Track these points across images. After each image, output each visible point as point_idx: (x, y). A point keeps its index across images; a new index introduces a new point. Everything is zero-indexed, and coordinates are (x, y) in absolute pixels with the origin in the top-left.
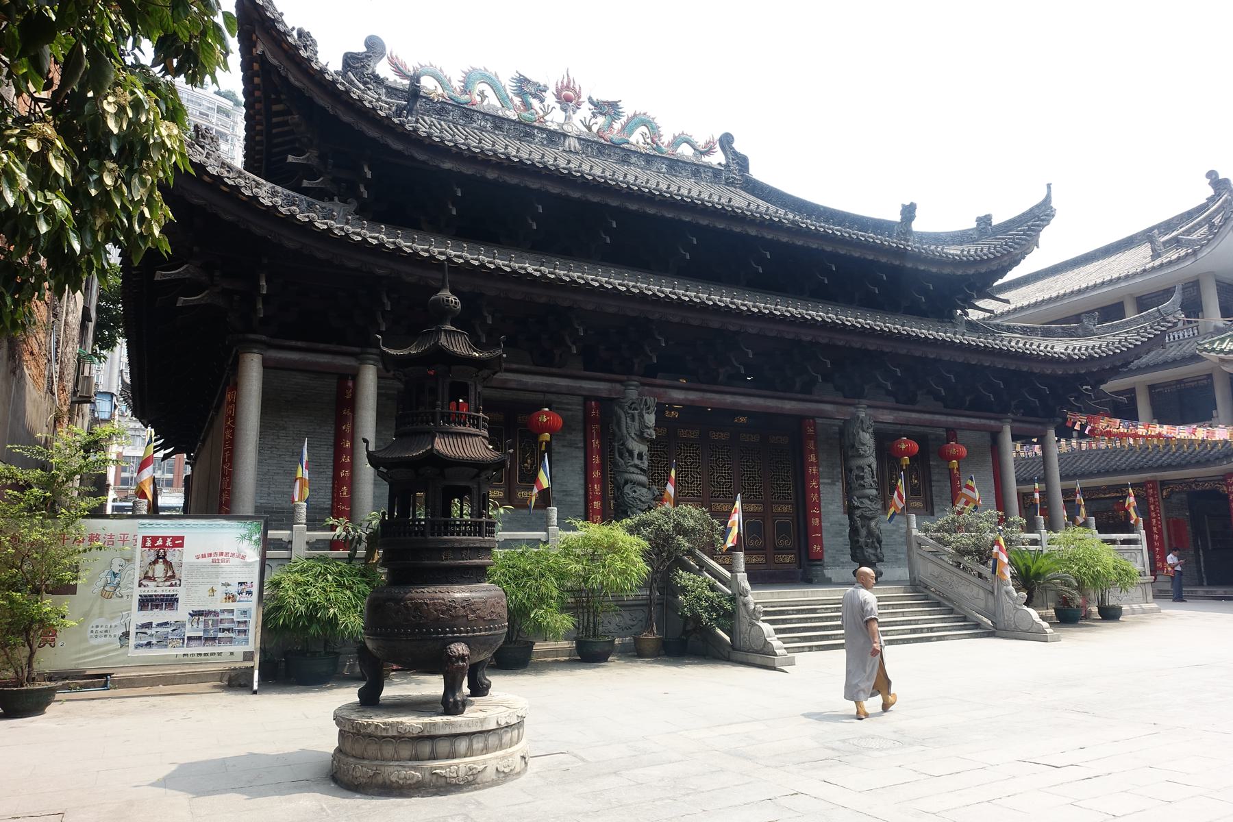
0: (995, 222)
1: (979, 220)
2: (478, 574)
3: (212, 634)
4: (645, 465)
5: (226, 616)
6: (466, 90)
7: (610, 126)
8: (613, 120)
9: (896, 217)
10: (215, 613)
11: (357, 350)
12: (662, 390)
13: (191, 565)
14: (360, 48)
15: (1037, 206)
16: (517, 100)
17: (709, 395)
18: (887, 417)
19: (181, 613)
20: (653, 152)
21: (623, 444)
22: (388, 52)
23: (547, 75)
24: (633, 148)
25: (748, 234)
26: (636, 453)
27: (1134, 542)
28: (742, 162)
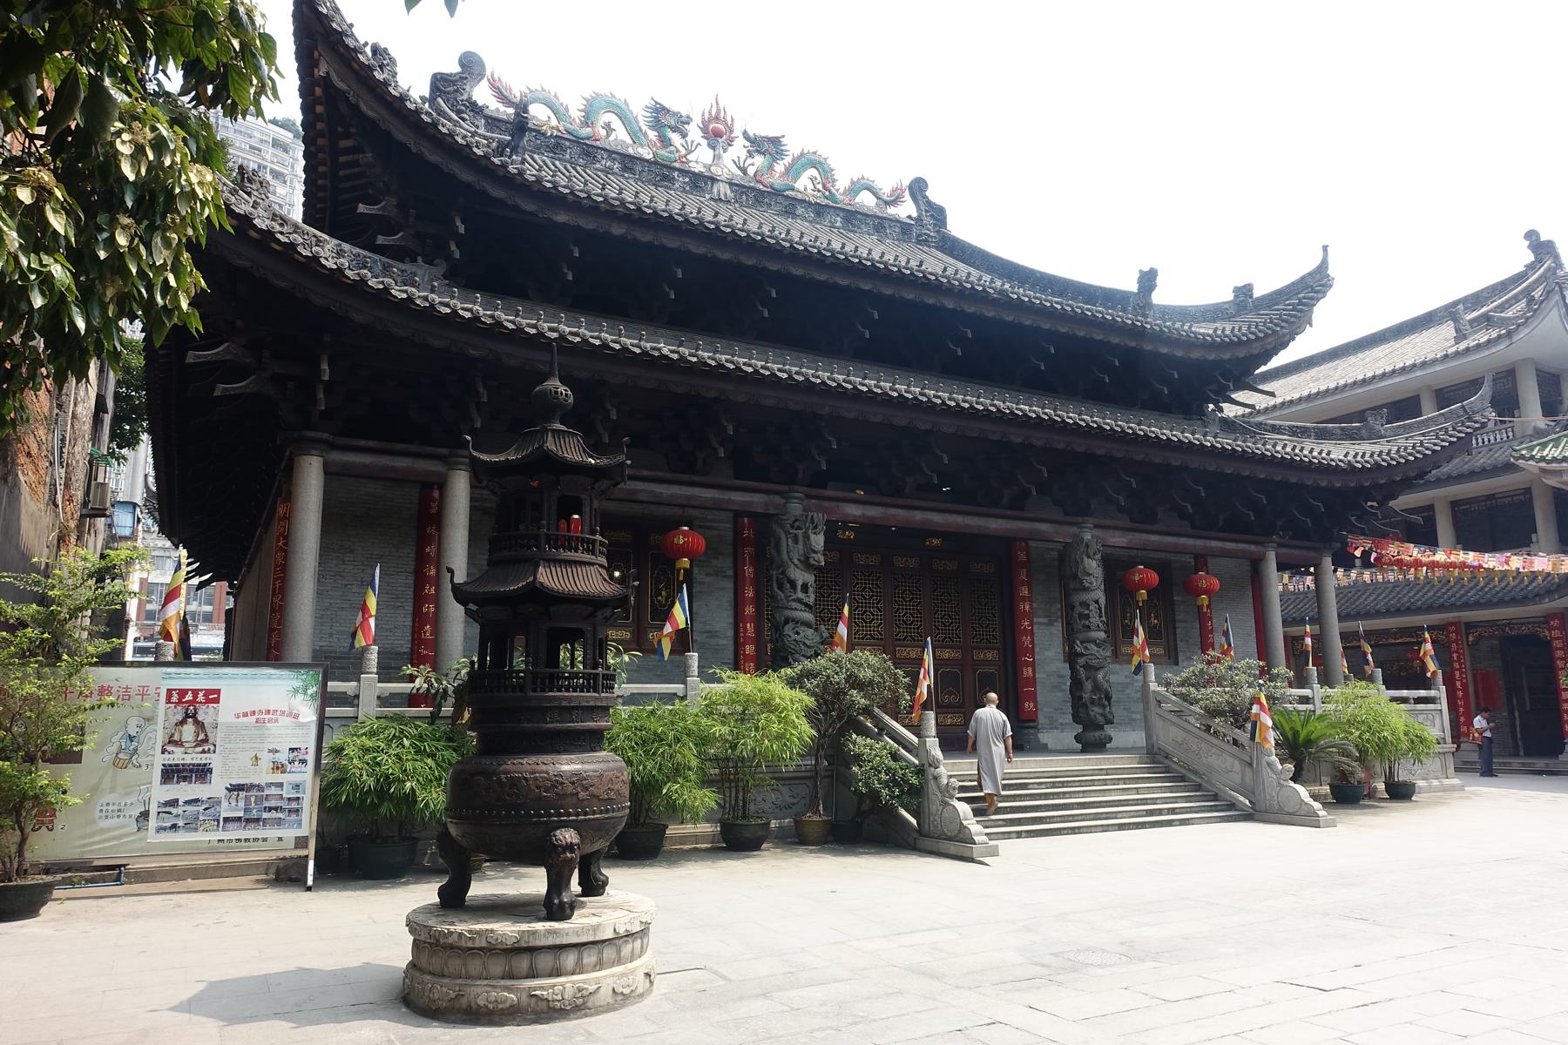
0: (1257, 293)
1: (1237, 290)
2: (592, 740)
3: (254, 814)
4: (811, 599)
5: (274, 791)
6: (587, 121)
7: (771, 168)
8: (775, 160)
9: (1133, 287)
10: (259, 788)
11: (445, 451)
12: (833, 504)
14: (454, 68)
15: (1310, 274)
16: (652, 135)
17: (893, 511)
18: (1119, 539)
19: (215, 787)
21: (783, 573)
22: (488, 73)
23: (691, 103)
24: (799, 196)
26: (800, 583)
28: (938, 214)
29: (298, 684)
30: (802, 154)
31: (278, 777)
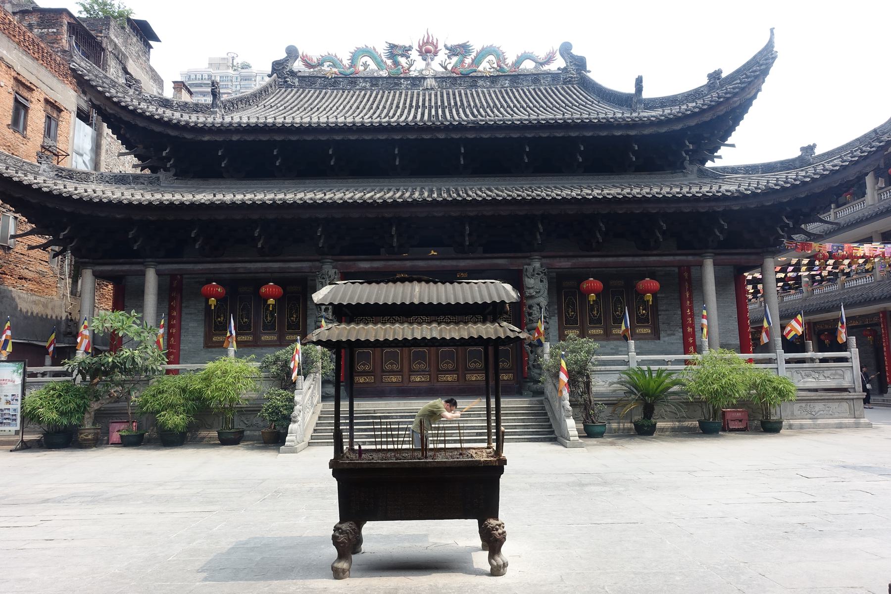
0: (724, 75)
5: (6, 412)
6: (353, 64)
7: (462, 62)
8: (465, 57)
9: (632, 90)
12: (351, 263)
14: (282, 55)
15: (760, 53)
16: (389, 62)
17: (391, 263)
18: (565, 264)
22: (300, 53)
23: (410, 38)
24: (480, 74)
25: (438, 139)
28: (580, 64)
29: (15, 368)
31: (8, 406)
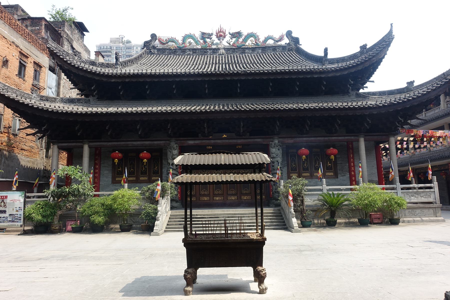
1: (361, 47)
3: (13, 220)
5: (16, 215)
7: (238, 41)
9: (322, 54)
10: (14, 215)
11: (81, 141)
13: (9, 203)
14: (149, 38)
15: (386, 36)
16: (202, 41)
17: (204, 141)
19: (7, 215)
20: (255, 46)
22: (158, 38)
23: (212, 29)
24: (246, 47)
26: (171, 164)
27: (430, 188)
28: (296, 41)
29: (21, 194)
30: (248, 34)
31: (17, 213)
